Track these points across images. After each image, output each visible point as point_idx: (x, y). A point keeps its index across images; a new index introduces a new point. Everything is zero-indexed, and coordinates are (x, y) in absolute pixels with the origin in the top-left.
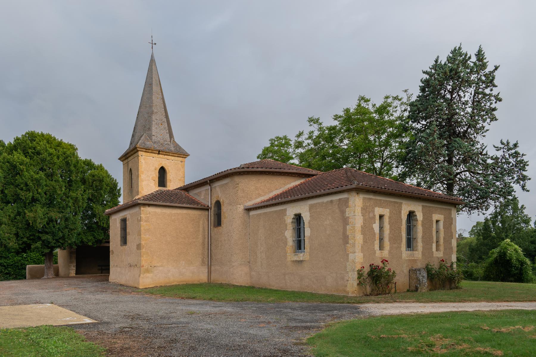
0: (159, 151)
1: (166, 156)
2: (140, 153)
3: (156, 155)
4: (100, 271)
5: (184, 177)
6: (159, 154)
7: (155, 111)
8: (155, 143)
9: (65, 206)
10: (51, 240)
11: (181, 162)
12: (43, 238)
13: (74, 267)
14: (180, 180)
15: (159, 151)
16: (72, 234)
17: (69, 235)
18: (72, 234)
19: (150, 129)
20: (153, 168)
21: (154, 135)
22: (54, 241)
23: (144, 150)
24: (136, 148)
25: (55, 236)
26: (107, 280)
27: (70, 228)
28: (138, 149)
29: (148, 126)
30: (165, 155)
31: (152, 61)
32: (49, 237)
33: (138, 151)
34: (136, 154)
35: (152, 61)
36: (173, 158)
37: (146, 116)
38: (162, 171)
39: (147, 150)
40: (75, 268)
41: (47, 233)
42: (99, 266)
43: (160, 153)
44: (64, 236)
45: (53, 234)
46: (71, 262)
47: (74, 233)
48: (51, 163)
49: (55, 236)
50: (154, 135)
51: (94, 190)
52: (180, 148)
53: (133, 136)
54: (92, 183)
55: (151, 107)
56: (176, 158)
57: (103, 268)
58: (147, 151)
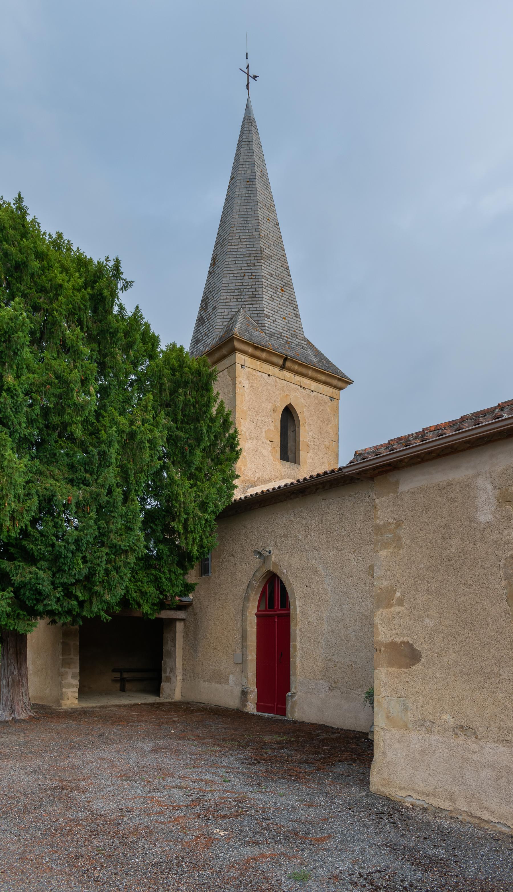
0: (286, 359)
1: (298, 378)
2: (239, 358)
3: (276, 371)
4: (118, 685)
5: (337, 442)
6: (283, 367)
7: (267, 251)
8: (272, 335)
9: (96, 460)
10: (47, 588)
11: (332, 398)
12: (17, 579)
13: (73, 677)
15: (286, 359)
16: (117, 569)
17: (107, 572)
18: (117, 569)
19: (254, 298)
20: (269, 407)
21: (267, 316)
22: (59, 593)
23: (250, 350)
24: (231, 339)
25: (60, 570)
26: (364, 781)
27: (113, 547)
28: (237, 344)
29: (249, 291)
30: (296, 373)
31: (248, 124)
32: (41, 574)
33: (234, 350)
34: (226, 362)
35: (248, 124)
37: (242, 263)
38: (289, 416)
39: (259, 351)
40: (76, 682)
41: (31, 559)
42: (114, 671)
43: (288, 364)
44: (89, 578)
45: (56, 563)
46: (66, 663)
47: (126, 564)
48: (43, 290)
49: (60, 570)
50: (267, 316)
51: (175, 420)
52: (328, 361)
53: (201, 321)
54: (173, 392)
55: (254, 239)
57: (125, 675)
58: (258, 353)
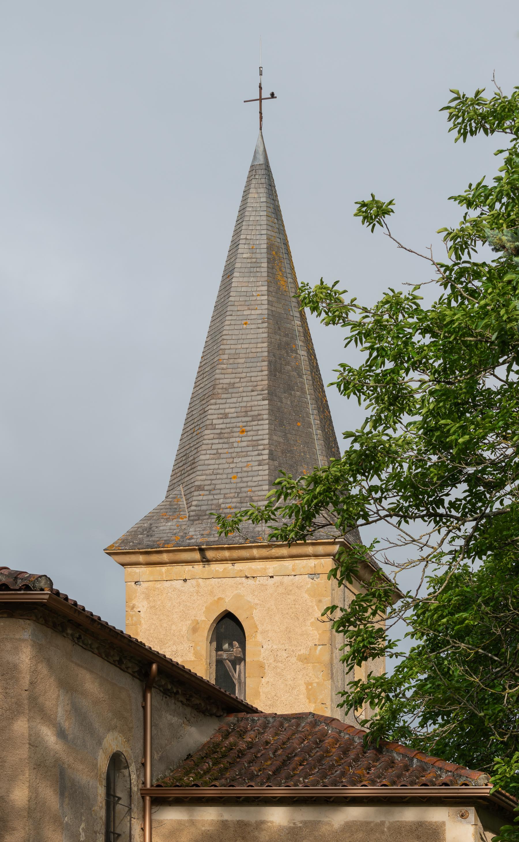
1: (239, 566)
3: (198, 568)
6: (206, 561)
14: (304, 659)
30: (234, 560)
36: (272, 566)
56: (289, 564)
